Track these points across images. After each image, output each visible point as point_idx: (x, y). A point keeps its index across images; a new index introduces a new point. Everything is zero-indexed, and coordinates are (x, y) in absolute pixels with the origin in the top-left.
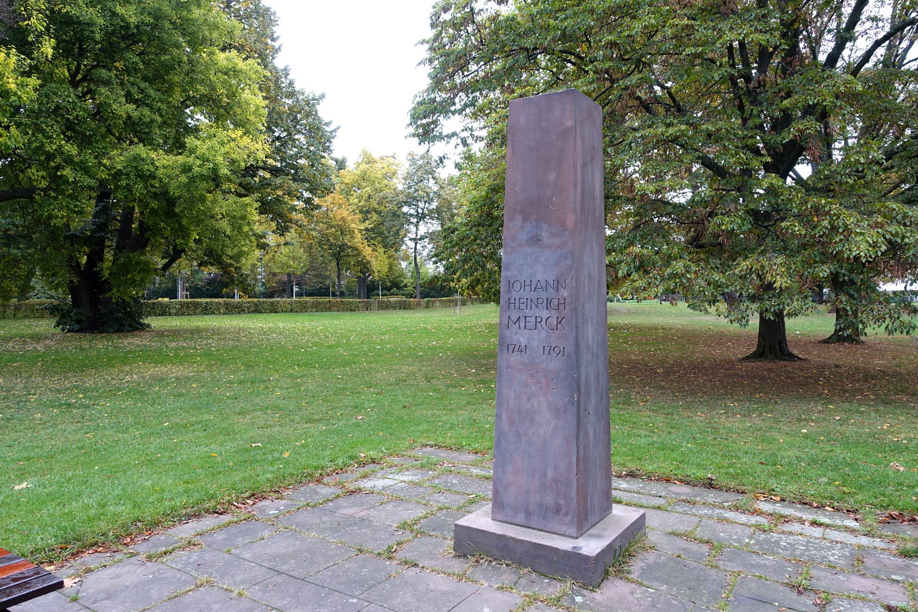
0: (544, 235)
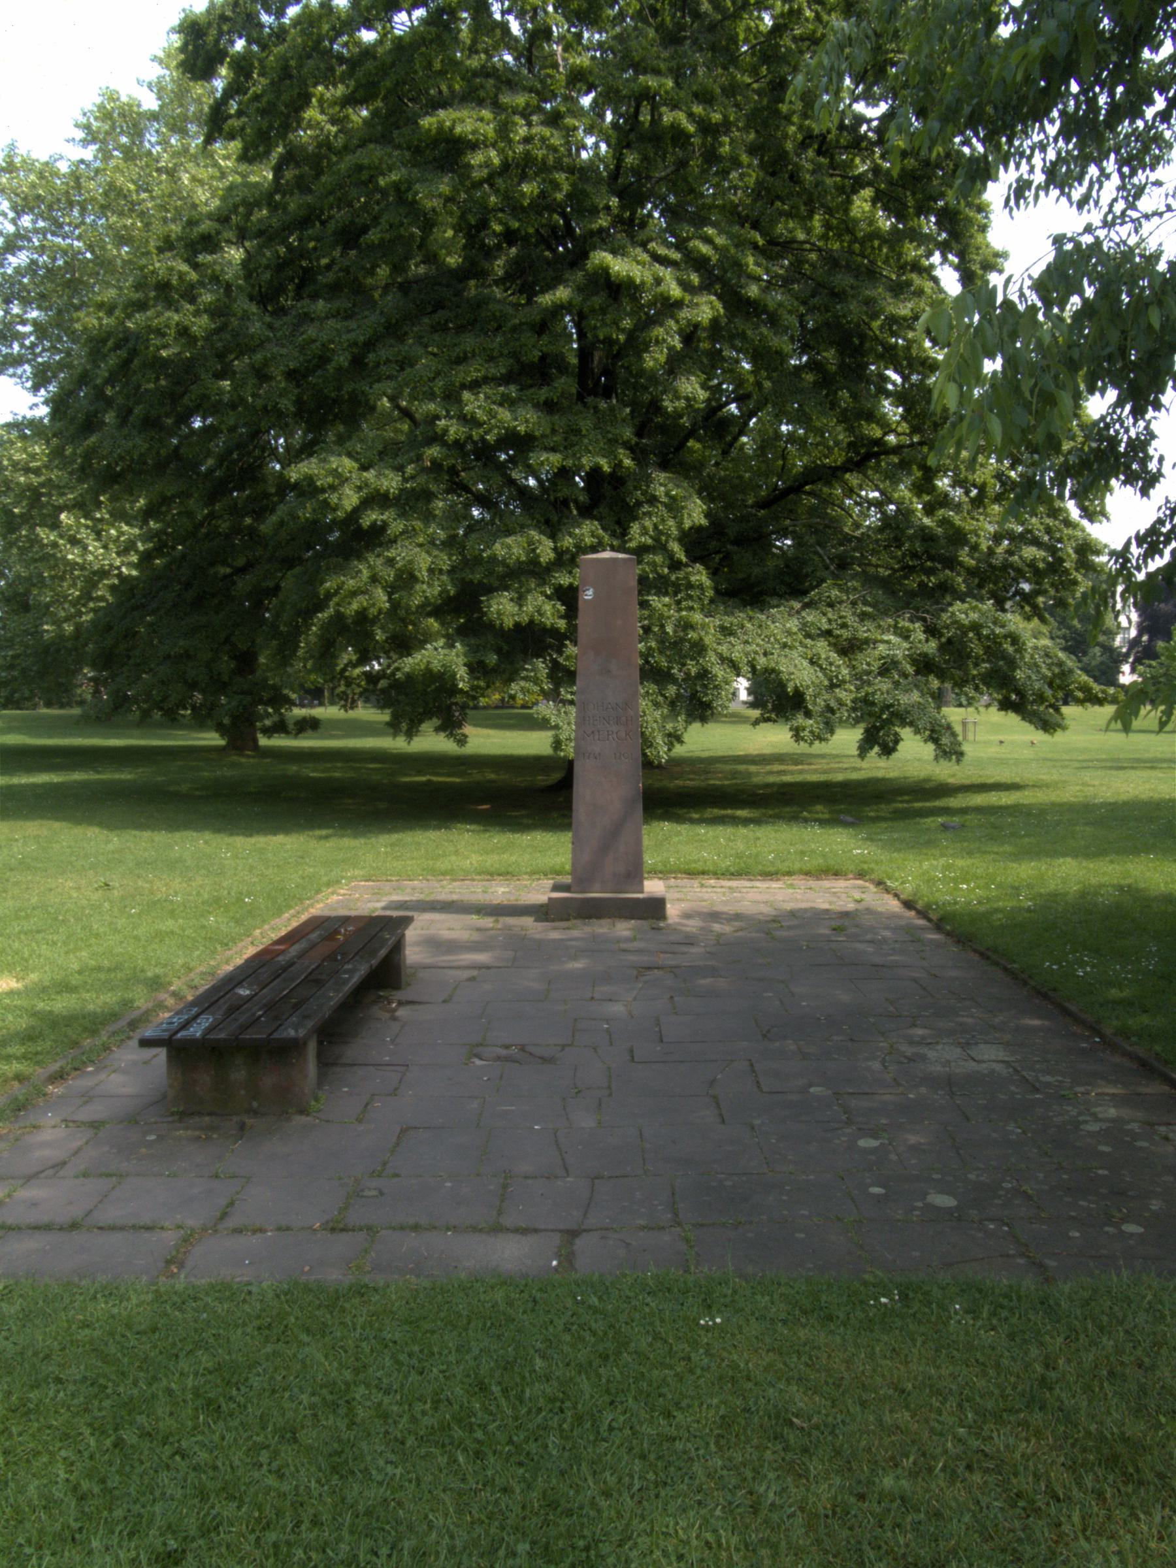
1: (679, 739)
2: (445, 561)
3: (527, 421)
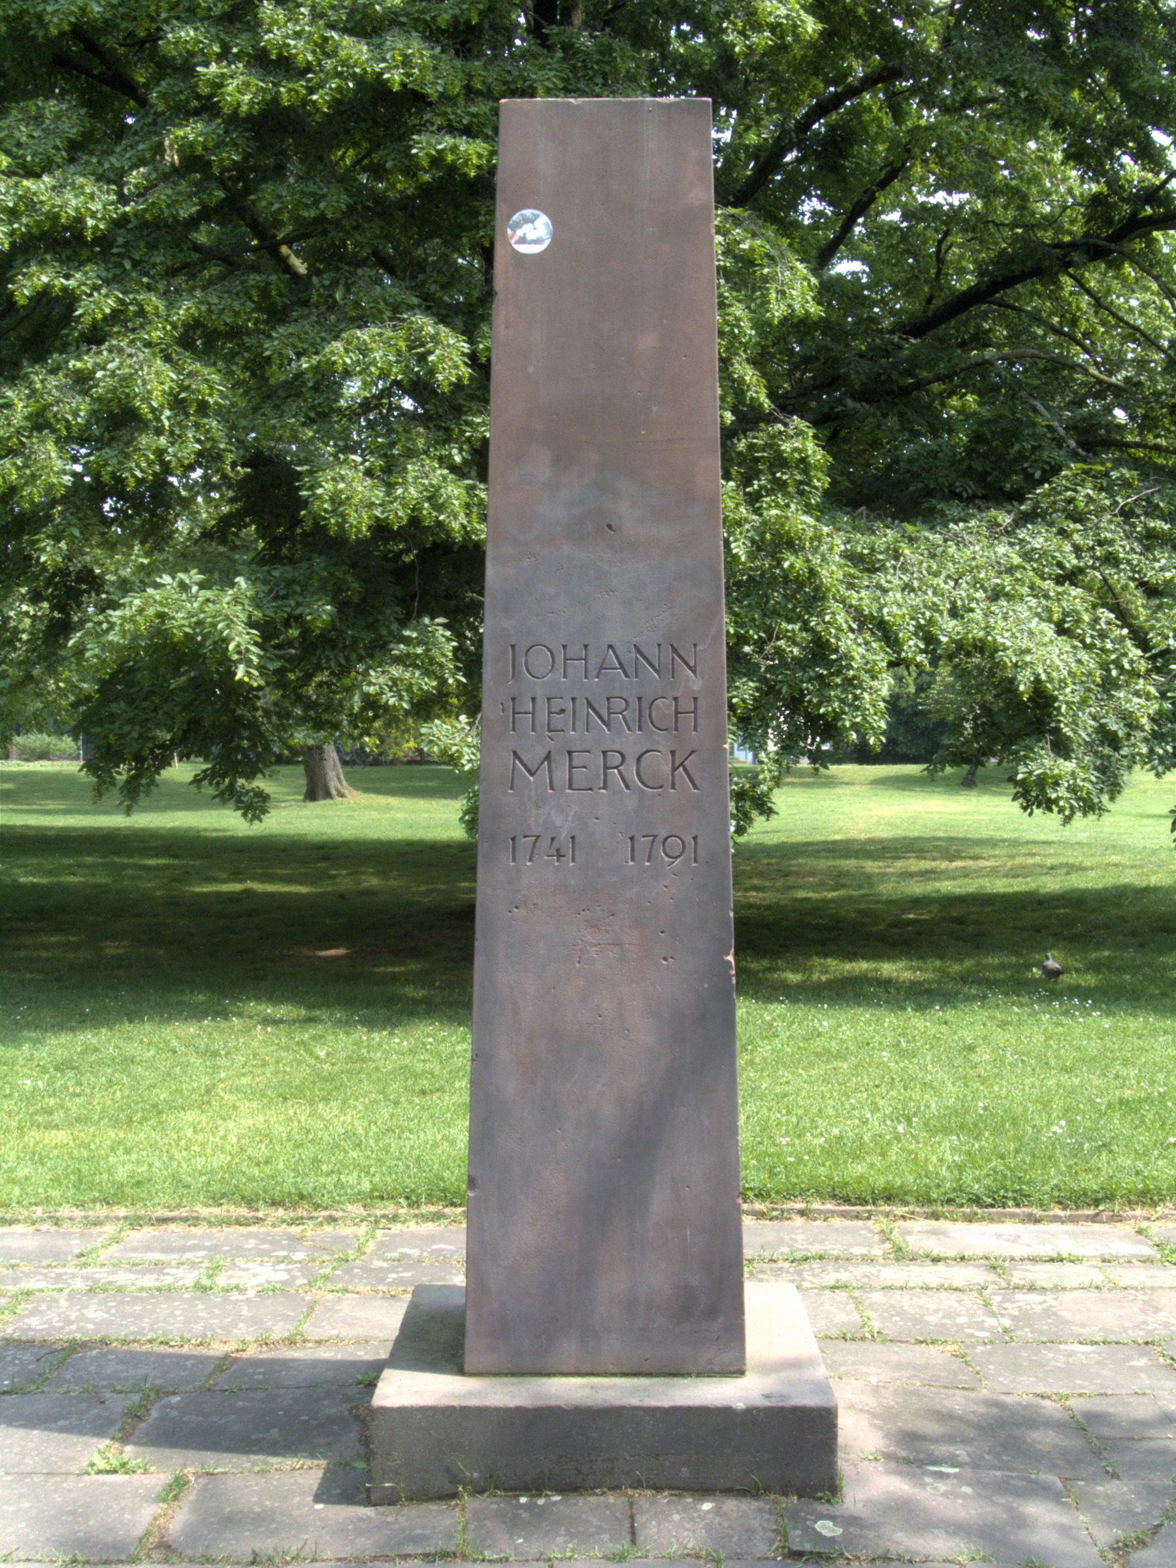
0: (626, 512)
1: (764, 807)
2: (211, 382)
3: (406, 62)
